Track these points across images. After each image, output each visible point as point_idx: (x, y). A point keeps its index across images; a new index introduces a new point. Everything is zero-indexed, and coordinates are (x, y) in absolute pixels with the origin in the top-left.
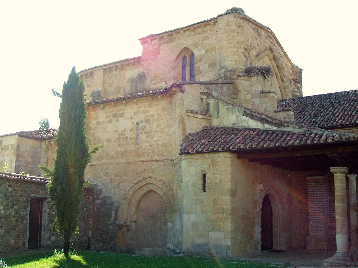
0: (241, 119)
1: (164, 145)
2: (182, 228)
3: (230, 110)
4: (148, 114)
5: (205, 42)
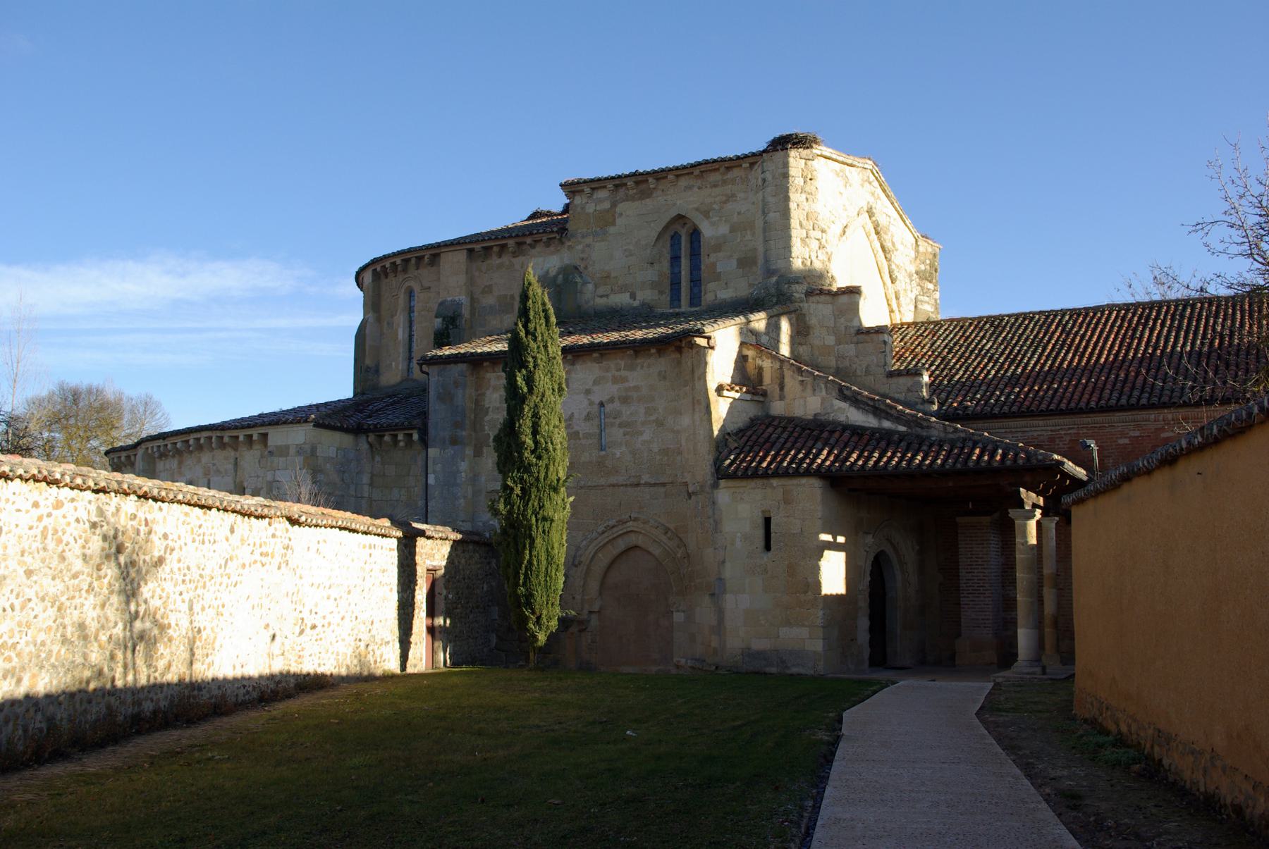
0: (832, 405)
1: (665, 452)
2: (721, 620)
3: (809, 386)
4: (626, 385)
5: (729, 206)
